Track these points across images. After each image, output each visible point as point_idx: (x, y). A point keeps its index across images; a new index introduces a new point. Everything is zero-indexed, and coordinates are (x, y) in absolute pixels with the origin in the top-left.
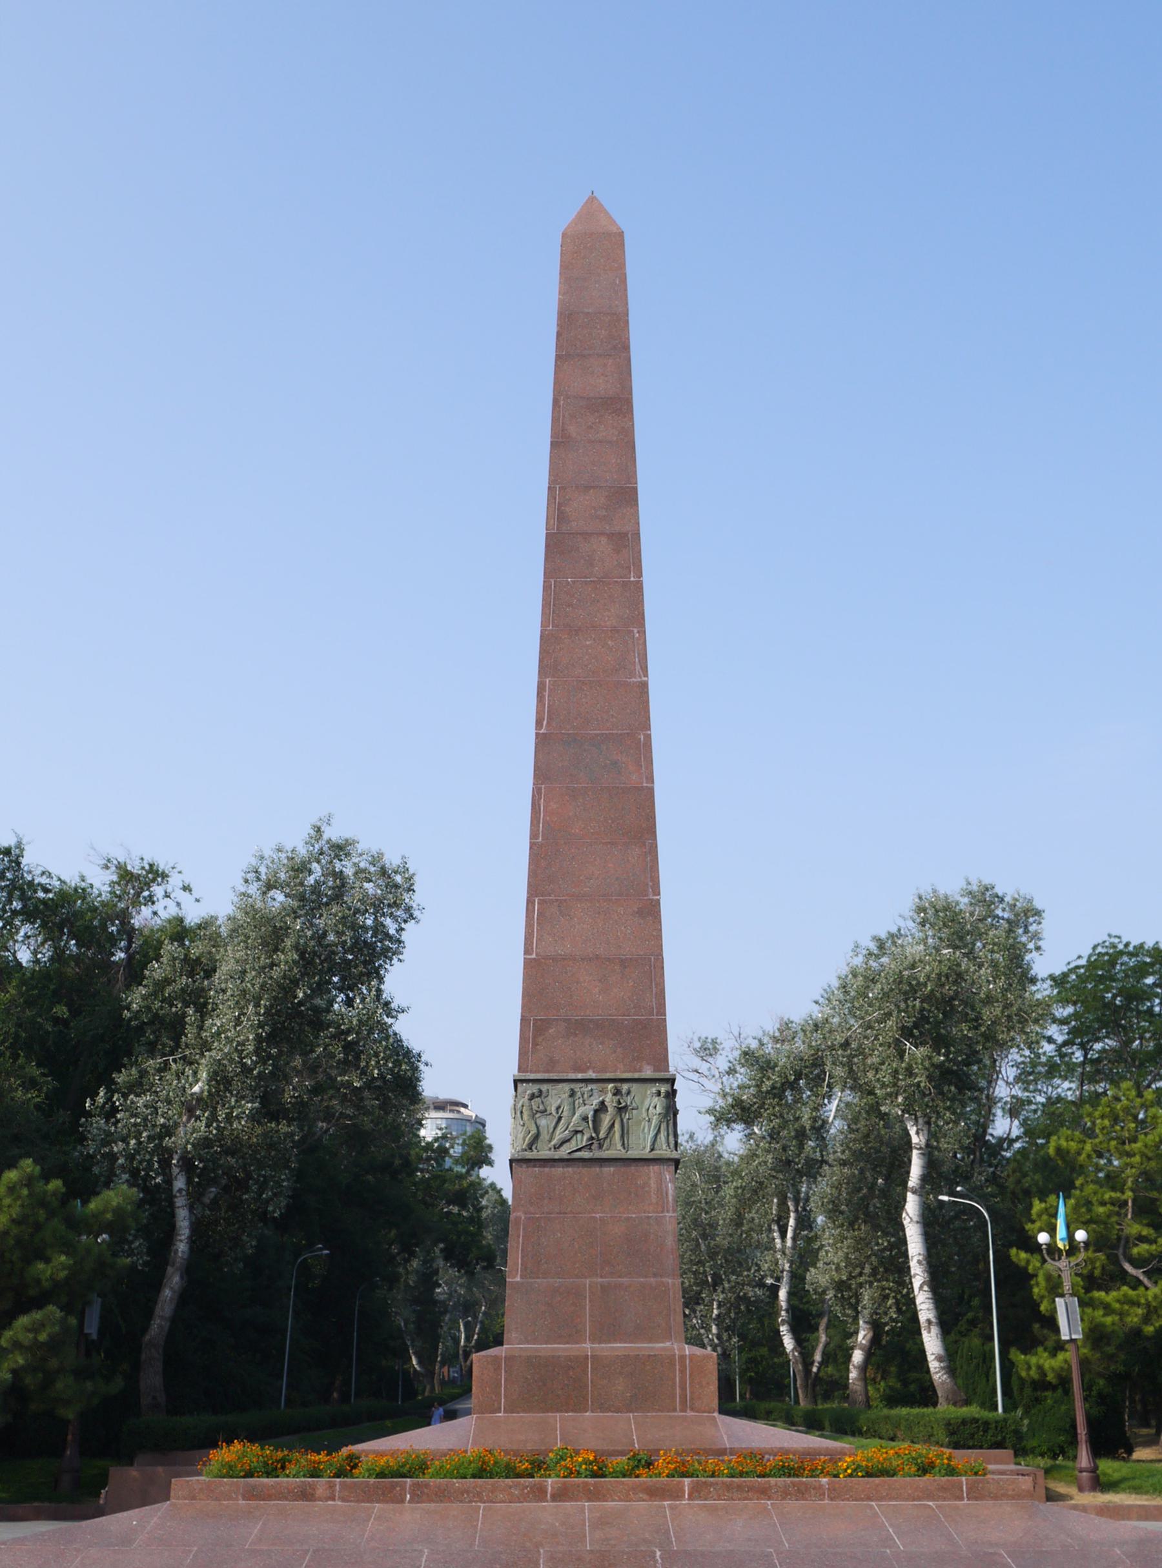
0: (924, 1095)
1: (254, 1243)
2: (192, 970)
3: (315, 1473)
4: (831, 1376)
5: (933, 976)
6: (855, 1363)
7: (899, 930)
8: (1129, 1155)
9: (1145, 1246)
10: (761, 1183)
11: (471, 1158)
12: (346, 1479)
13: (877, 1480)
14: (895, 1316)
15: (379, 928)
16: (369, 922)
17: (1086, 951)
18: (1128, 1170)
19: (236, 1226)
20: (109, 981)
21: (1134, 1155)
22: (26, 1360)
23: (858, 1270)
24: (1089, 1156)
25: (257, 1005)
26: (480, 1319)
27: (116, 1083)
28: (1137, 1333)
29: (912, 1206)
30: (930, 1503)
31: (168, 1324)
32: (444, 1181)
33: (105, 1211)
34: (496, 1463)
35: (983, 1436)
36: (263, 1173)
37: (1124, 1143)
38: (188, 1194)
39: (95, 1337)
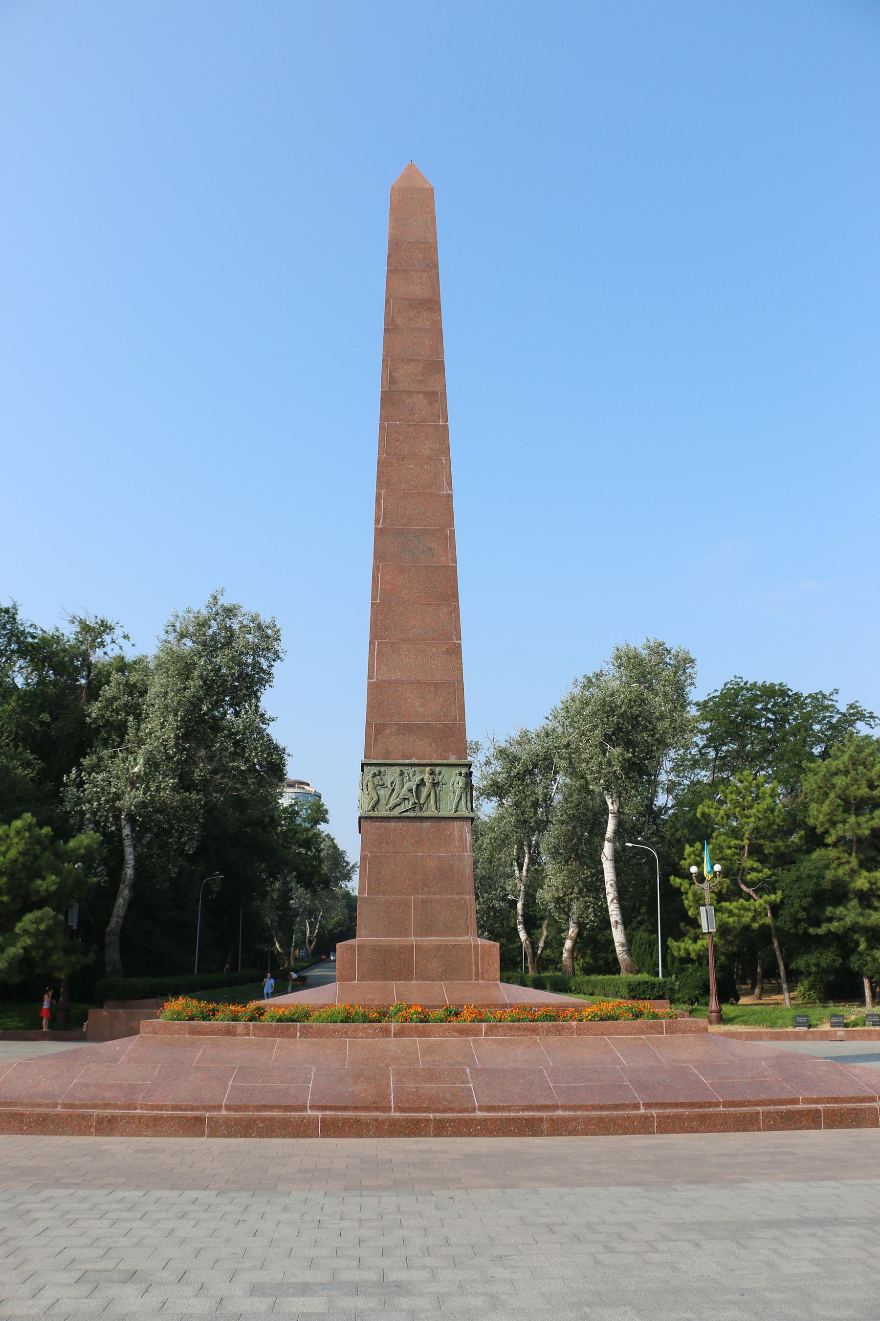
0: (618, 779)
1: (176, 870)
2: (131, 691)
3: (235, 1019)
4: (549, 956)
5: (626, 701)
6: (567, 948)
7: (601, 671)
8: (747, 817)
9: (755, 874)
10: (507, 835)
11: (314, 818)
12: (256, 1022)
13: (608, 1023)
14: (593, 919)
15: (256, 665)
16: (249, 661)
17: (720, 687)
18: (746, 827)
19: (164, 859)
20: (76, 697)
21: (751, 817)
22: (33, 941)
23: (570, 890)
24: (722, 818)
25: (176, 715)
26: (319, 920)
27: (82, 765)
28: (747, 928)
29: (607, 849)
30: (642, 1037)
31: (122, 920)
32: (296, 833)
33: (79, 848)
34: (356, 1013)
35: (650, 992)
36: (181, 825)
37: (744, 810)
38: (132, 838)
39: (75, 928)
